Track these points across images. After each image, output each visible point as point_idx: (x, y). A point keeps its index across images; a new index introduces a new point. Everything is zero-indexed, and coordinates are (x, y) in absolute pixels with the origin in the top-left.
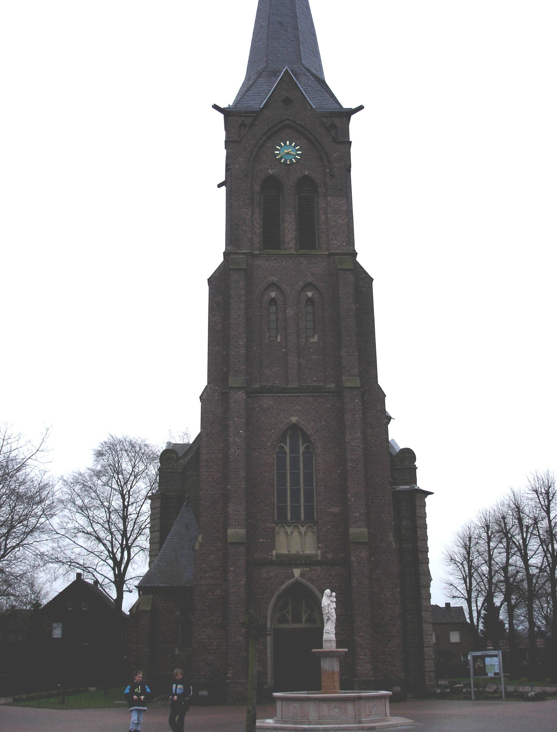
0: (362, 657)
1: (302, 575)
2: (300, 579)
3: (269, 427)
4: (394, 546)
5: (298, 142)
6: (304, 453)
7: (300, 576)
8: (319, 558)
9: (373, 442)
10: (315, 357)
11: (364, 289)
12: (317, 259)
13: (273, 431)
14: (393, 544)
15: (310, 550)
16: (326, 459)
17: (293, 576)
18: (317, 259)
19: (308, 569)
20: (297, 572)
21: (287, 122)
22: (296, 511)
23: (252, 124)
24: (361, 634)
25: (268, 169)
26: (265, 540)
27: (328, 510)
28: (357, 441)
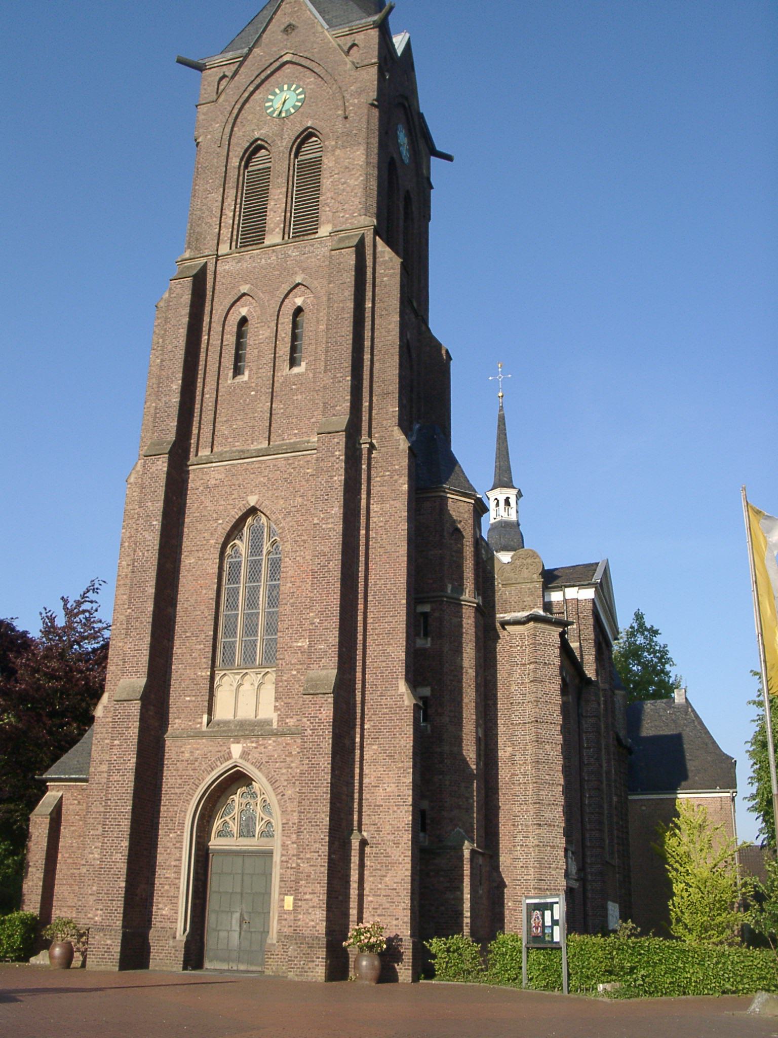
0: (307, 897)
1: (245, 755)
2: (240, 761)
3: (215, 515)
4: (407, 703)
5: (301, 83)
6: (269, 553)
7: (241, 757)
8: (275, 725)
9: (381, 524)
10: (299, 397)
11: (385, 279)
12: (313, 246)
13: (220, 522)
14: (405, 697)
15: (268, 712)
16: (298, 558)
17: (229, 756)
18: (313, 246)
19: (254, 745)
20: (236, 750)
21: (285, 59)
22: (250, 648)
23: (236, 73)
24: (308, 856)
25: (253, 131)
26: (193, 698)
27: (295, 644)
28: (332, 520)
